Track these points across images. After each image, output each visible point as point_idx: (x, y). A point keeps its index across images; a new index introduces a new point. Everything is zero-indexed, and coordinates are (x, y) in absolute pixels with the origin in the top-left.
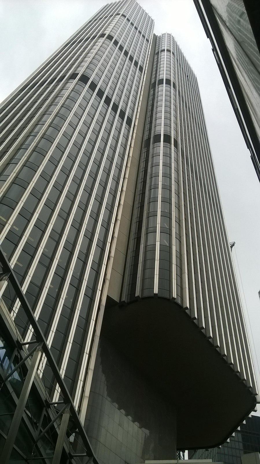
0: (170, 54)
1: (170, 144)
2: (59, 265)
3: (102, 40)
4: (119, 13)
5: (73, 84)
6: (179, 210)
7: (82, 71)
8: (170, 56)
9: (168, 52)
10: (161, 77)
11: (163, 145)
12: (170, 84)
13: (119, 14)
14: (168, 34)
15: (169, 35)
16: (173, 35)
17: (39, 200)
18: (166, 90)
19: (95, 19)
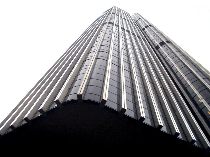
0: (149, 28)
1: (164, 44)
2: (128, 100)
3: (106, 26)
4: (106, 22)
5: (88, 70)
6: (188, 60)
7: (84, 79)
8: (150, 29)
9: (147, 28)
10: (143, 28)
11: (184, 75)
12: (164, 44)
13: (106, 23)
14: (134, 14)
15: (135, 14)
16: (135, 12)
17: (107, 61)
18: (165, 50)
19: (96, 27)
